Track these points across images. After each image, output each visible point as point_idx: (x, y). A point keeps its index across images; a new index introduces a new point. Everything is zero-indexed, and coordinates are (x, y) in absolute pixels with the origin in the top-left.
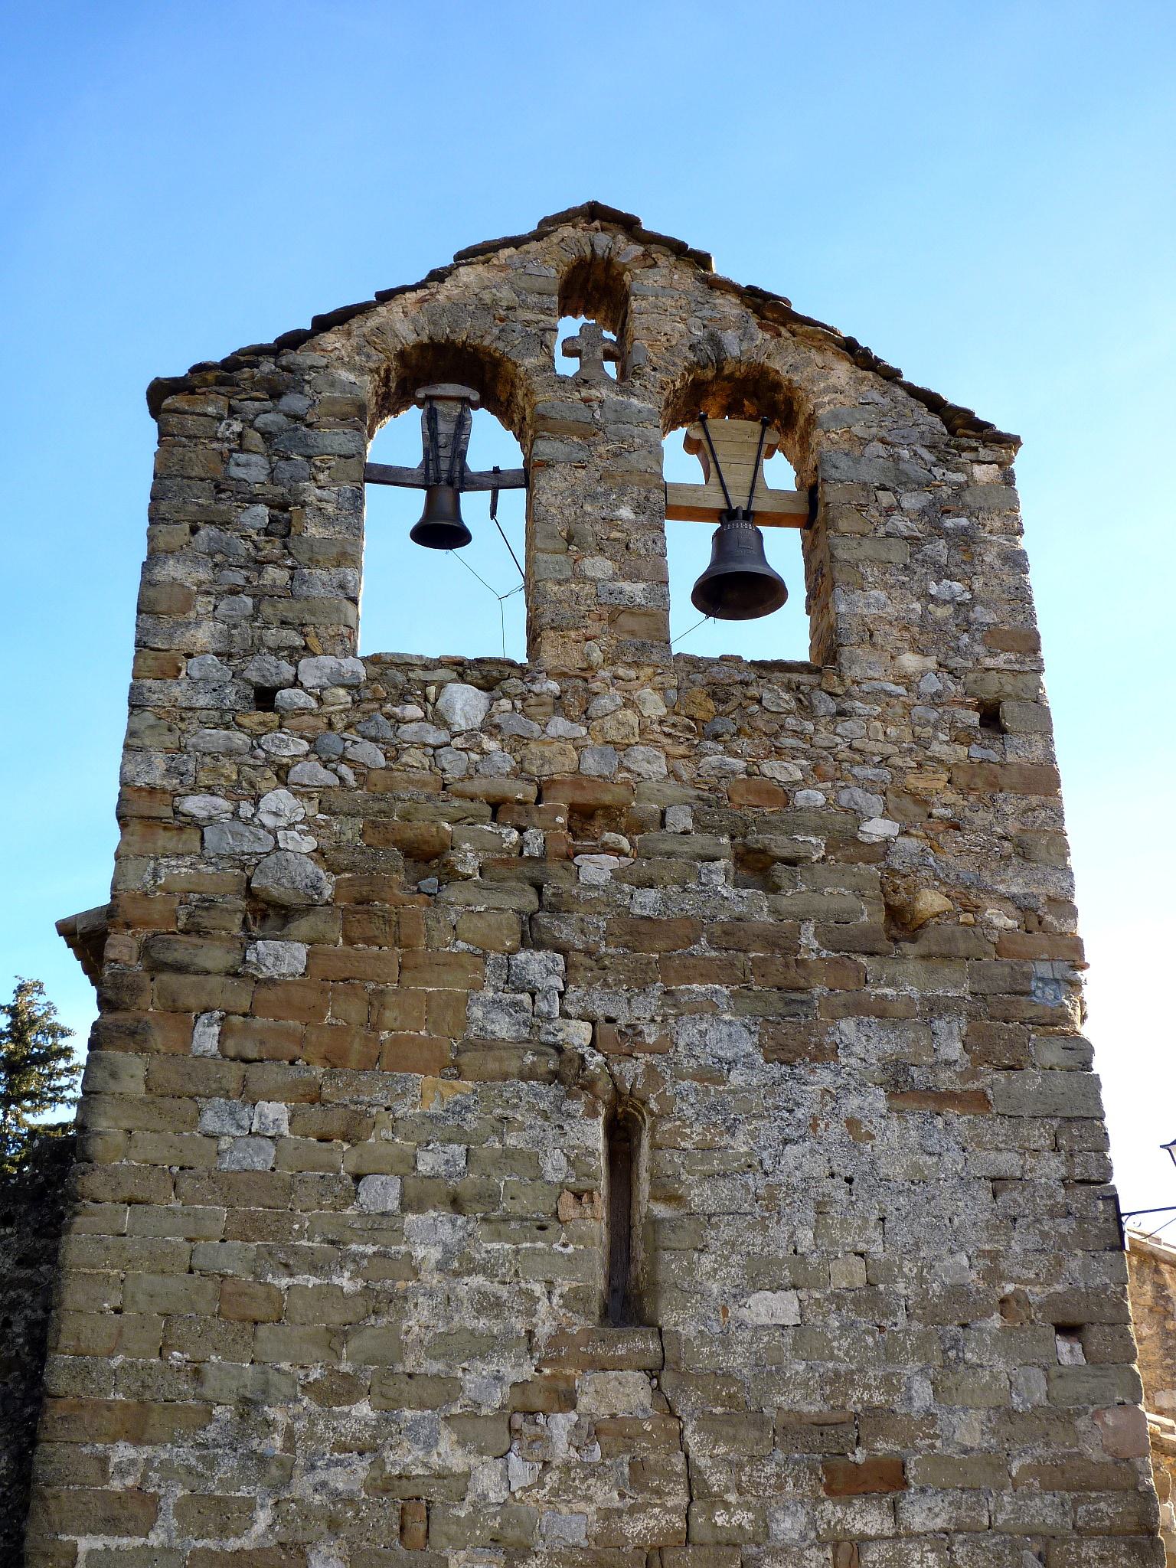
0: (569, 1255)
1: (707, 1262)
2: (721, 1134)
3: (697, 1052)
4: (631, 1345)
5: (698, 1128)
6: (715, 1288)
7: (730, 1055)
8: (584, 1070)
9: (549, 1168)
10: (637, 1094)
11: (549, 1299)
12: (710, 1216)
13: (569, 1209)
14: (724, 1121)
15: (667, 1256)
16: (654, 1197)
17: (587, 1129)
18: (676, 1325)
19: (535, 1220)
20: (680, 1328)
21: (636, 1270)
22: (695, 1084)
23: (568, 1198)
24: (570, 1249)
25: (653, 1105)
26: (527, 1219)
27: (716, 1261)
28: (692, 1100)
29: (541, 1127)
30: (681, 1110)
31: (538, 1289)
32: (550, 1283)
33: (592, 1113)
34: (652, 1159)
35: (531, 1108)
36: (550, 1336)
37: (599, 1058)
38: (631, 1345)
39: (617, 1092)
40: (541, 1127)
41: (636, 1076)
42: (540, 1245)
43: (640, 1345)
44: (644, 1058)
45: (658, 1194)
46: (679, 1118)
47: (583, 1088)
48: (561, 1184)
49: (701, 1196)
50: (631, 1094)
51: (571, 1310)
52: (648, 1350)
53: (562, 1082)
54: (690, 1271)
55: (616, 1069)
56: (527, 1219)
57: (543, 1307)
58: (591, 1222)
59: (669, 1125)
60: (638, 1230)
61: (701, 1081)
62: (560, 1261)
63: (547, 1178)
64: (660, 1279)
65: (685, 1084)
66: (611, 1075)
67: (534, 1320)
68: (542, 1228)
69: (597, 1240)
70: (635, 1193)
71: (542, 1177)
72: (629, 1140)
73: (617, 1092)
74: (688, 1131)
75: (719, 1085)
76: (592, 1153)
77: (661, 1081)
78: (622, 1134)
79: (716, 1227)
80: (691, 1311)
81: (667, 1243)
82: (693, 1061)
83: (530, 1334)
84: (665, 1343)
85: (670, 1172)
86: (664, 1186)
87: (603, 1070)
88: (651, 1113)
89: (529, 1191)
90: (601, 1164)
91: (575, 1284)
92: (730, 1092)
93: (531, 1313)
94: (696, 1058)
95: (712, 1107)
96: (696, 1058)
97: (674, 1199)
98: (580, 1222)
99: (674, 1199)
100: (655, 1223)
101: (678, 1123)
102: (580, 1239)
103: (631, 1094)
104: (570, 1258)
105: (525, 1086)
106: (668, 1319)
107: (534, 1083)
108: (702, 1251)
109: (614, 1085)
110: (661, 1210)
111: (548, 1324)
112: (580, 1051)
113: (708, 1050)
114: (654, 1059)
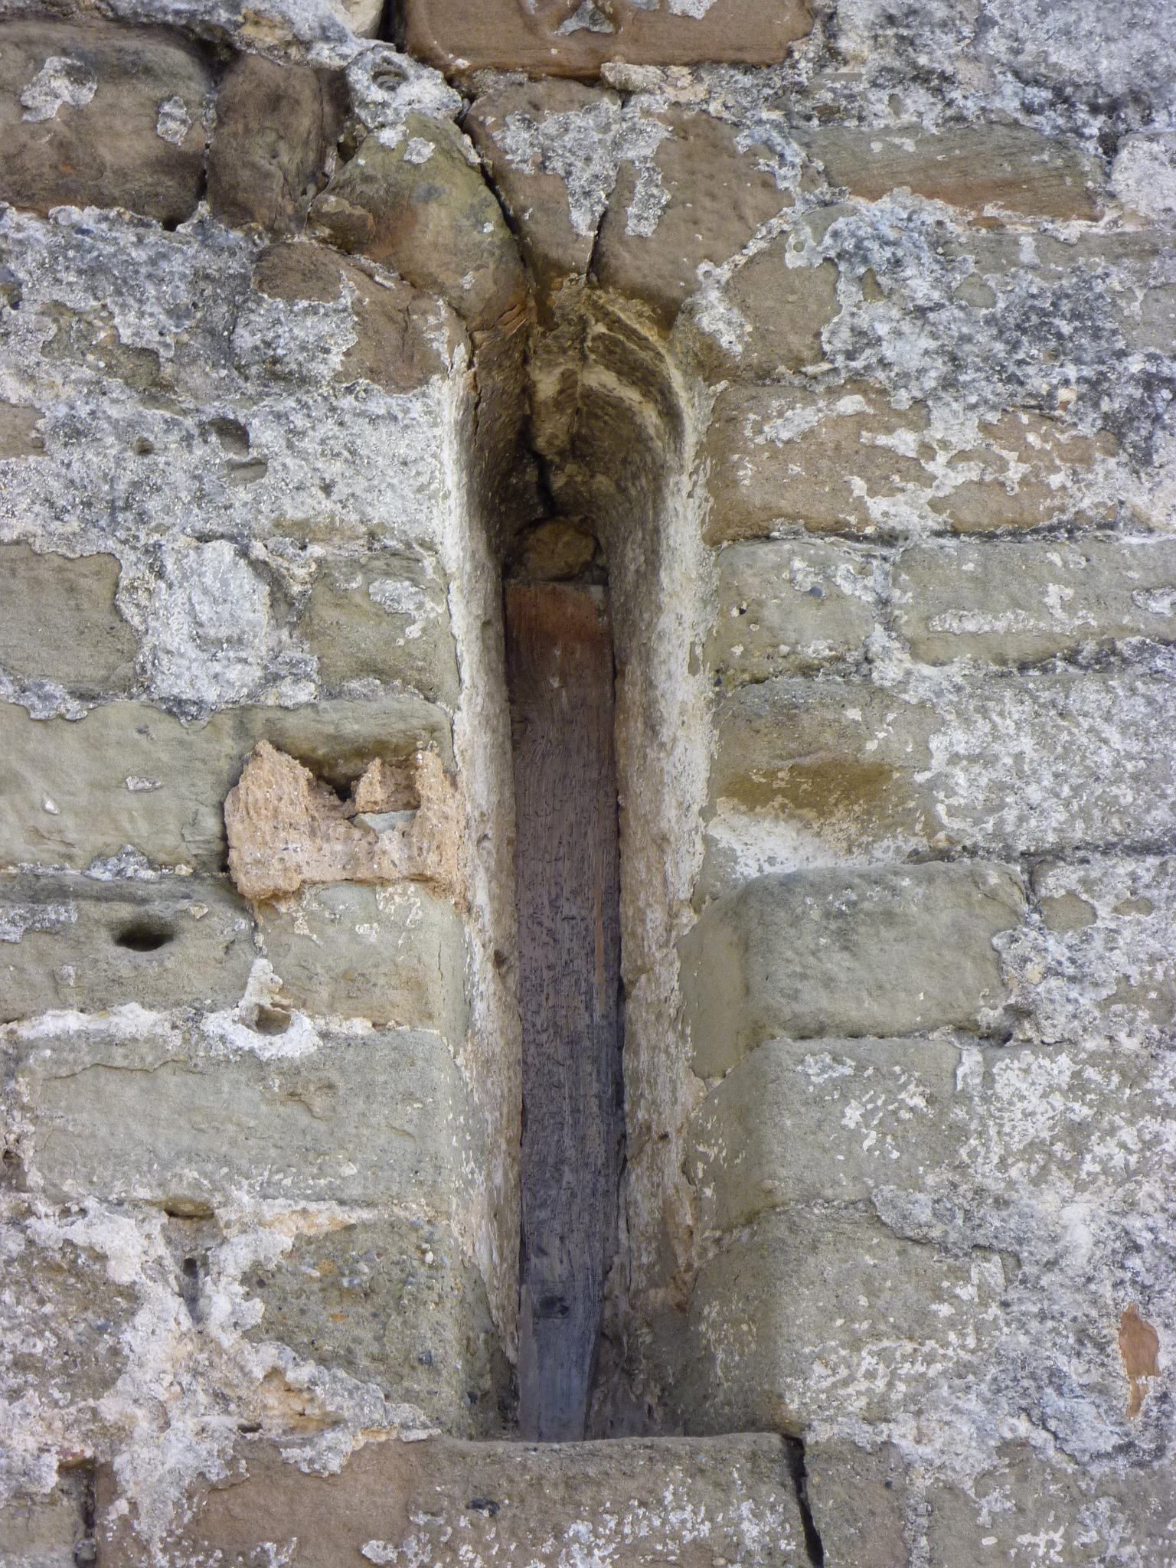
0: (291, 1070)
1: (1029, 1091)
2: (1080, 458)
3: (939, 52)
4: (640, 1525)
5: (955, 425)
6: (1079, 1221)
7: (1113, 67)
8: (346, 153)
9: (174, 633)
10: (628, 264)
11: (192, 1298)
12: (1037, 862)
13: (282, 832)
14: (1095, 388)
15: (815, 1066)
16: (740, 788)
17: (371, 439)
18: (878, 1413)
19: (105, 895)
20: (902, 1433)
21: (656, 1187)
22: (933, 211)
23: (279, 784)
24: (299, 1040)
25: (718, 318)
26: (61, 893)
27: (1078, 1087)
28: (921, 286)
29: (124, 430)
30: (865, 339)
31: (130, 1246)
32: (191, 1216)
33: (402, 364)
34: (723, 593)
35: (71, 336)
36: (202, 1487)
37: (426, 91)
38: (640, 1525)
39: (527, 257)
40: (124, 430)
41: (623, 182)
42: (134, 1019)
43: (689, 1521)
44: (665, 90)
45: (760, 757)
46: (857, 382)
47: (348, 240)
48: (242, 714)
49: (981, 760)
50: (598, 266)
51: (311, 1351)
52: (734, 1547)
53: (234, 209)
54: (942, 1138)
55: (516, 142)
56: (61, 893)
57: (155, 1336)
58: (406, 901)
59: (804, 417)
60: (662, 981)
61: (966, 195)
62: (245, 1100)
63: (170, 683)
64: (786, 1175)
65: (878, 214)
66: (492, 178)
67: (110, 1407)
68: (143, 937)
69: (441, 995)
70: (638, 785)
71: (137, 682)
72: (597, 569)
73: (527, 257)
74: (905, 441)
75: (1063, 214)
76: (404, 558)
77: (754, 198)
78: (556, 513)
79: (1076, 912)
80: (959, 1346)
81: (814, 1001)
82: (917, 99)
83: (89, 1479)
84: (823, 1508)
85: (817, 648)
86: (788, 714)
87: (447, 151)
88: (709, 362)
89: (69, 748)
90: (450, 611)
91: (326, 1217)
92: (1119, 248)
93: (92, 1370)
94: (936, 82)
95: (1032, 323)
96: (936, 82)
97: (838, 786)
98: (348, 899)
99: (838, 786)
100: (745, 910)
101: (850, 404)
102: (352, 987)
103: (598, 266)
104: (296, 1084)
105: (34, 228)
106: (833, 1385)
107: (86, 216)
108: (999, 1038)
109: (511, 222)
110: (768, 847)
111: (184, 1425)
112: (325, 54)
113: (996, 44)
114: (716, 94)
